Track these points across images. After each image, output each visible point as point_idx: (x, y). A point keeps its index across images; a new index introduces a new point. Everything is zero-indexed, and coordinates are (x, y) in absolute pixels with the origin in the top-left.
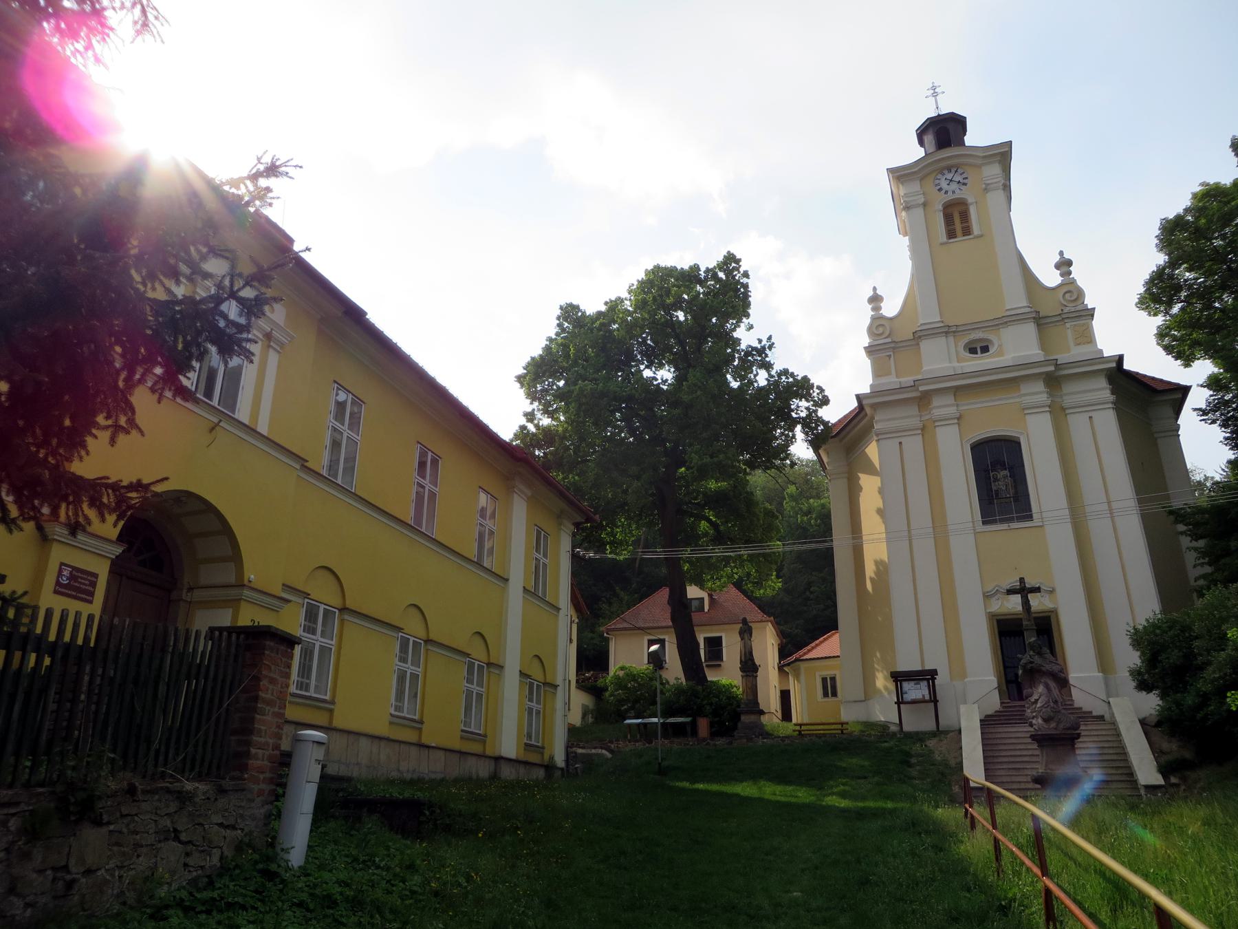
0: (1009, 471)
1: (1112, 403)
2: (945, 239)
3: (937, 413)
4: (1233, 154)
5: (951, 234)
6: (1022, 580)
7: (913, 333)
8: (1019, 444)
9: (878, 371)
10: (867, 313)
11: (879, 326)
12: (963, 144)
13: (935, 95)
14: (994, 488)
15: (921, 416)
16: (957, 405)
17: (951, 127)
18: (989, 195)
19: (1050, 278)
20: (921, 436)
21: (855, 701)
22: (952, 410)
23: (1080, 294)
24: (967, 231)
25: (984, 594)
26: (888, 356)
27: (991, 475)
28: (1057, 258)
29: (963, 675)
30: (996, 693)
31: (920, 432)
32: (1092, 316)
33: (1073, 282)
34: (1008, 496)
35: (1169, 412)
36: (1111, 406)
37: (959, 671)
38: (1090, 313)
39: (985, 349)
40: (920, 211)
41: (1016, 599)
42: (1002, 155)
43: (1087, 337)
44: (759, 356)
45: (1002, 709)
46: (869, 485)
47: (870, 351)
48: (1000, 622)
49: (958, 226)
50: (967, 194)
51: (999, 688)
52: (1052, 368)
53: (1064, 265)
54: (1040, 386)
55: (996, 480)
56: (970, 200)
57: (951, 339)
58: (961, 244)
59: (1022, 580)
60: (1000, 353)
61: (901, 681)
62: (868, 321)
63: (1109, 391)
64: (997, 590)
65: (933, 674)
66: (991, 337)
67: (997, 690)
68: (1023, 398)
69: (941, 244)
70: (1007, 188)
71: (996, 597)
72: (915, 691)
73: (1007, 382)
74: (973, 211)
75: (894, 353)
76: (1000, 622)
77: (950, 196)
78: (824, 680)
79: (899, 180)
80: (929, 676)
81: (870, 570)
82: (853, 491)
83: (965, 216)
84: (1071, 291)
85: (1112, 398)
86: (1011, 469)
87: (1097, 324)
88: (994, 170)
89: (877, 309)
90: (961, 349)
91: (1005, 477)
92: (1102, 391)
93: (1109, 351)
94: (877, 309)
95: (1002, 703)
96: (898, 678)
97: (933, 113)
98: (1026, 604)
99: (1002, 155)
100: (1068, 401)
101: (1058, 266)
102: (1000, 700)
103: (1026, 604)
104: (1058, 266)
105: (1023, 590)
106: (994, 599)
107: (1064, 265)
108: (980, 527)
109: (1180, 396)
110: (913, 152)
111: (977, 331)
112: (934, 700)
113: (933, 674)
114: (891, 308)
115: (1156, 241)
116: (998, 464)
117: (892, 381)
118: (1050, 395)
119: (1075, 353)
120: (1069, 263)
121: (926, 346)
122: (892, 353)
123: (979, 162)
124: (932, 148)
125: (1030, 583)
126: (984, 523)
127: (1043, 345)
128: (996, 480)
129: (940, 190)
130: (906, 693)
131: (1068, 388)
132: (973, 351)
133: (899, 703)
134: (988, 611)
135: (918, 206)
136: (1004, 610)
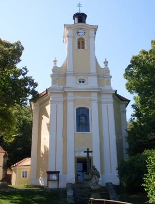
4: (52, 73)
5: (79, 47)
6: (88, 149)
8: (88, 110)
9: (53, 82)
10: (53, 65)
11: (55, 69)
12: (85, 22)
13: (79, 6)
17: (83, 17)
19: (102, 66)
22: (73, 98)
23: (109, 71)
24: (83, 48)
28: (104, 60)
29: (66, 173)
33: (108, 68)
35: (124, 106)
37: (65, 173)
38: (111, 77)
39: (83, 82)
40: (71, 39)
41: (86, 154)
42: (95, 29)
43: (109, 83)
44: (19, 72)
46: (46, 120)
47: (52, 76)
49: (81, 45)
52: (99, 90)
53: (106, 63)
54: (95, 95)
56: (85, 39)
59: (88, 149)
60: (87, 84)
62: (52, 67)
65: (58, 172)
70: (95, 37)
72: (54, 177)
73: (89, 92)
77: (80, 37)
78: (23, 172)
80: (57, 173)
81: (42, 150)
82: (40, 119)
83: (83, 43)
84: (107, 70)
85: (113, 101)
86: (86, 117)
87: (112, 80)
89: (55, 64)
90: (77, 80)
92: (110, 98)
93: (114, 88)
94: (55, 64)
96: (49, 173)
97: (78, 12)
98: (88, 155)
99: (95, 29)
101: (104, 63)
103: (88, 155)
104: (104, 63)
105: (88, 152)
107: (106, 63)
110: (71, 22)
112: (58, 180)
113: (58, 172)
114: (59, 65)
115: (33, 78)
116: (83, 115)
117: (57, 86)
118: (98, 98)
119: (106, 87)
120: (107, 62)
124: (77, 22)
125: (90, 150)
126: (77, 131)
127: (99, 83)
131: (103, 96)
132: (80, 82)
133: (48, 180)
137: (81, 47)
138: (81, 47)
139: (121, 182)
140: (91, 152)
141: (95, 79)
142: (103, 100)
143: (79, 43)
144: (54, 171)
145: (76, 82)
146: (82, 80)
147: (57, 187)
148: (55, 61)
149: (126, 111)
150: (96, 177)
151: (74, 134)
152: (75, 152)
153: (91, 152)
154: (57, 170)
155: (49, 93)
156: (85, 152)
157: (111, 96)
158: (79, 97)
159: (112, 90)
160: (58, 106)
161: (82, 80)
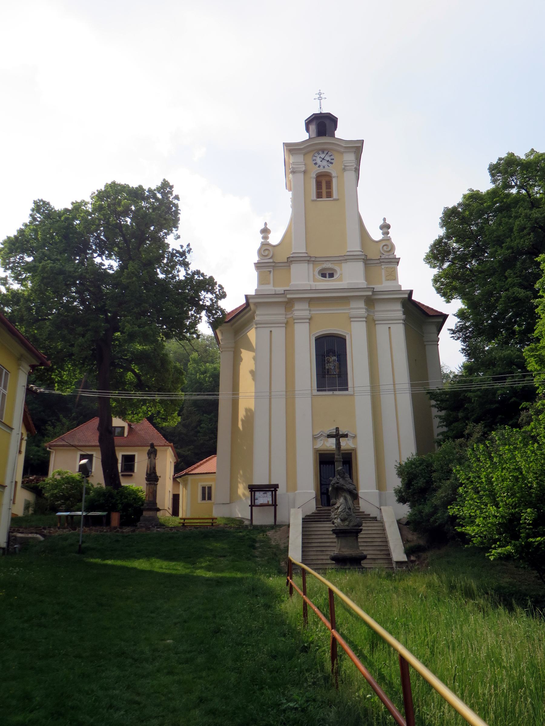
0: (337, 357)
1: (403, 320)
2: (315, 198)
3: (297, 314)
5: (319, 195)
6: (337, 429)
7: (288, 258)
8: (345, 340)
9: (262, 281)
10: (258, 240)
12: (333, 135)
13: (320, 99)
14: (327, 367)
15: (286, 315)
16: (310, 310)
17: (327, 122)
18: (346, 173)
19: (376, 235)
20: (284, 328)
21: (223, 504)
22: (306, 313)
25: (313, 436)
26: (269, 271)
27: (326, 358)
28: (382, 222)
30: (314, 502)
31: (284, 325)
32: (398, 263)
33: (389, 239)
34: (335, 373)
36: (402, 321)
37: (292, 486)
38: (397, 261)
39: (331, 275)
40: (301, 176)
43: (393, 276)
45: (316, 512)
48: (321, 455)
50: (333, 170)
51: (316, 498)
52: (370, 293)
53: (385, 227)
54: (361, 304)
55: (329, 362)
56: (334, 174)
57: (311, 266)
58: (324, 203)
59: (337, 429)
60: (340, 279)
61: (255, 491)
62: (259, 246)
63: (401, 312)
64: (321, 434)
65: (276, 487)
66: (336, 267)
67: (315, 499)
68: (351, 311)
69: (313, 201)
70: (357, 170)
71: (320, 439)
72: (263, 498)
74: (334, 182)
75: (273, 269)
76: (321, 455)
77: (321, 170)
78: (204, 488)
79: (290, 152)
80: (272, 489)
82: (236, 360)
83: (329, 185)
85: (403, 317)
86: (338, 356)
88: (350, 157)
89: (265, 238)
90: (316, 273)
91: (334, 361)
93: (405, 287)
94: (265, 238)
95: (317, 508)
96: (253, 489)
97: (317, 112)
98: (338, 444)
100: (378, 315)
101: (382, 228)
102: (316, 505)
103: (338, 444)
104: (382, 228)
105: (338, 436)
106: (319, 440)
107: (385, 227)
108: (315, 392)
109: (441, 320)
111: (327, 263)
113: (276, 487)
116: (331, 352)
117: (270, 288)
119: (384, 285)
120: (388, 227)
121: (295, 268)
122: (272, 270)
123: (342, 150)
125: (342, 431)
127: (367, 278)
128: (329, 362)
129: (316, 164)
130: (257, 499)
131: (379, 307)
132: (324, 275)
133: (252, 506)
134: (315, 447)
135: (300, 172)
136: (324, 448)
137: (324, 194)
138: (324, 194)
139: (468, 299)
140: (346, 436)
141: (360, 266)
142: (378, 315)
143: (319, 185)
144: (266, 483)
145: (314, 275)
146: (327, 273)
147: (273, 524)
148: (265, 231)
149: (438, 345)
150: (349, 497)
151: (313, 396)
152: (315, 438)
153: (346, 436)
154: (273, 482)
155: (252, 306)
156: (330, 436)
157: (398, 307)
158: (319, 311)
159: (400, 291)
160: (273, 332)
161: (327, 273)
